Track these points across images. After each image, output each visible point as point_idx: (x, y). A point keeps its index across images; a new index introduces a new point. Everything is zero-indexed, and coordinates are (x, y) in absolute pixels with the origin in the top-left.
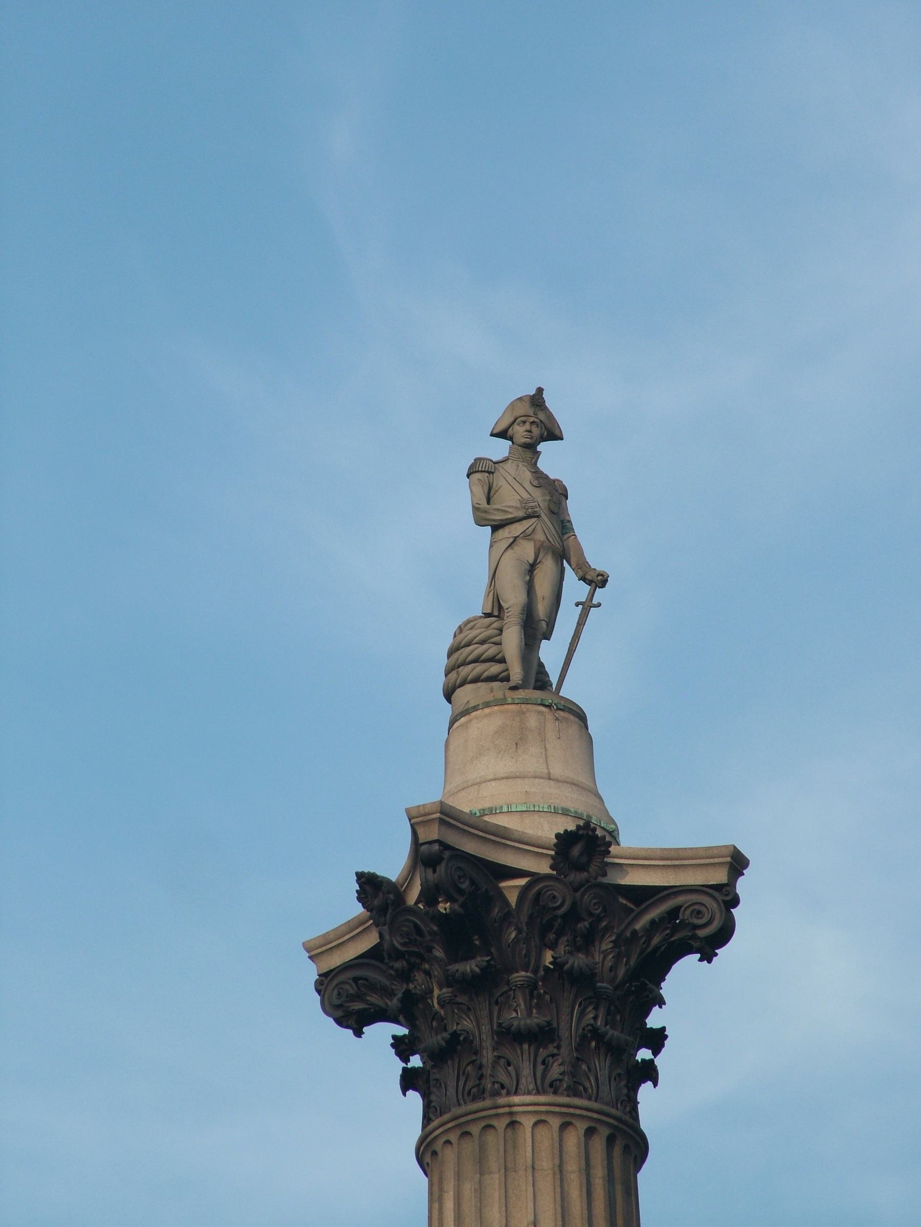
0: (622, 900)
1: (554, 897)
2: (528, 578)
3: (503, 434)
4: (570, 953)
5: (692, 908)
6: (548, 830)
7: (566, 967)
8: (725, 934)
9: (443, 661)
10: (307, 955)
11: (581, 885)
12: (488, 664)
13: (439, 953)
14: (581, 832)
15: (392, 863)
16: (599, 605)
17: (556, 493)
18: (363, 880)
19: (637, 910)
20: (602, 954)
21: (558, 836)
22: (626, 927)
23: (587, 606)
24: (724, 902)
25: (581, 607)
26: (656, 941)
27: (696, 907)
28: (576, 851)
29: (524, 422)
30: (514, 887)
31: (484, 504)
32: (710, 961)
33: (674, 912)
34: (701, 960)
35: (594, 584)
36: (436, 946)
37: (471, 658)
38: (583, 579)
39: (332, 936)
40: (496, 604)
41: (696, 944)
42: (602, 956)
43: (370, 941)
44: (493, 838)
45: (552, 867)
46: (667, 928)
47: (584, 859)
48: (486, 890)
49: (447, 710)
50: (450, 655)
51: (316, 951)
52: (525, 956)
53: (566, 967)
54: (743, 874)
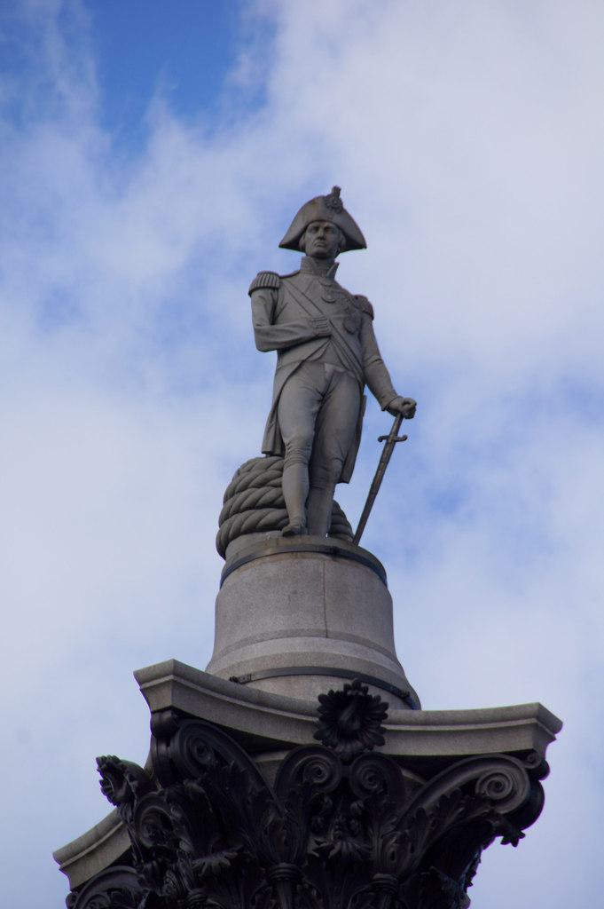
0: (406, 774)
1: (319, 772)
2: (316, 408)
3: (293, 244)
4: (341, 838)
5: (489, 781)
6: (309, 692)
7: (332, 853)
8: (530, 811)
9: (218, 507)
10: (59, 866)
11: (354, 756)
12: (265, 511)
13: (185, 846)
14: (349, 693)
15: (137, 749)
16: (405, 438)
17: (359, 312)
18: (104, 766)
19: (426, 785)
20: (384, 841)
21: (322, 698)
22: (412, 807)
23: (391, 441)
24: (529, 771)
25: (384, 441)
26: (450, 820)
27: (496, 779)
28: (345, 716)
29: (317, 229)
30: (275, 762)
31: (266, 326)
32: (515, 844)
33: (469, 787)
34: (504, 843)
35: (399, 416)
36: (184, 839)
37: (245, 504)
38: (387, 408)
39: (84, 843)
40: (278, 441)
41: (496, 823)
42: (381, 841)
43: (124, 844)
44: (228, 699)
45: (316, 737)
46: (458, 807)
47: (356, 725)
48: (235, 767)
49: (220, 563)
50: (226, 499)
51: (69, 860)
52: (286, 842)
53: (332, 853)
54: (554, 739)
